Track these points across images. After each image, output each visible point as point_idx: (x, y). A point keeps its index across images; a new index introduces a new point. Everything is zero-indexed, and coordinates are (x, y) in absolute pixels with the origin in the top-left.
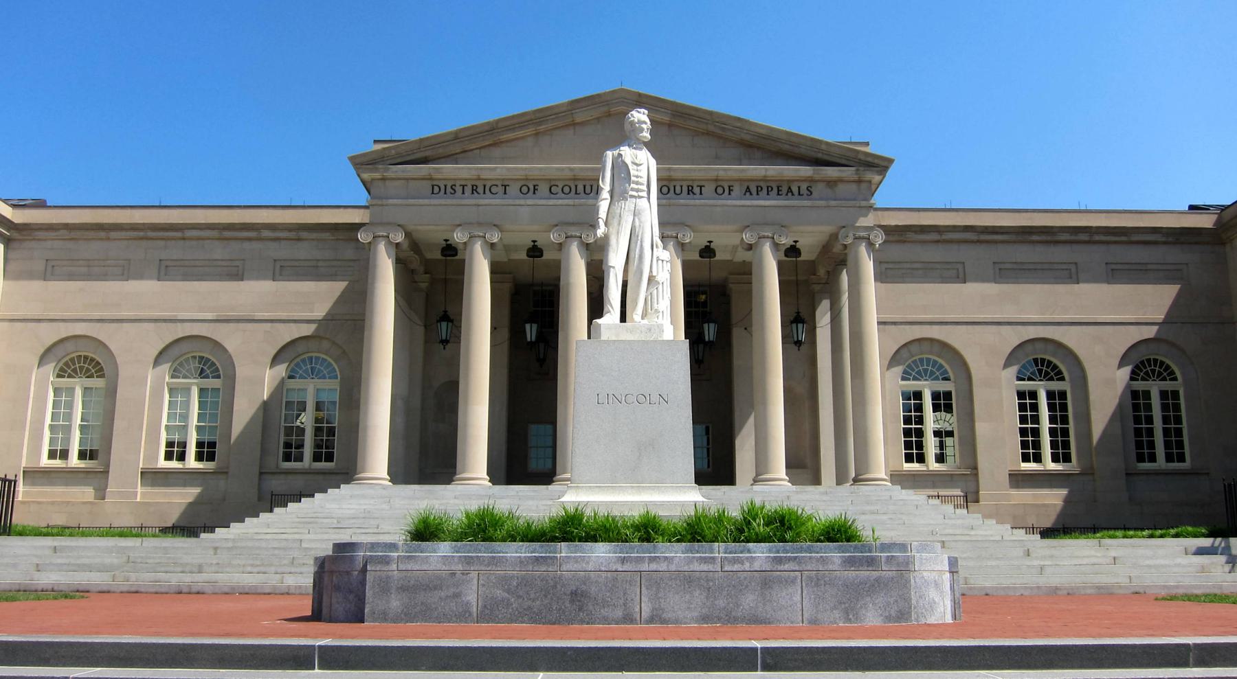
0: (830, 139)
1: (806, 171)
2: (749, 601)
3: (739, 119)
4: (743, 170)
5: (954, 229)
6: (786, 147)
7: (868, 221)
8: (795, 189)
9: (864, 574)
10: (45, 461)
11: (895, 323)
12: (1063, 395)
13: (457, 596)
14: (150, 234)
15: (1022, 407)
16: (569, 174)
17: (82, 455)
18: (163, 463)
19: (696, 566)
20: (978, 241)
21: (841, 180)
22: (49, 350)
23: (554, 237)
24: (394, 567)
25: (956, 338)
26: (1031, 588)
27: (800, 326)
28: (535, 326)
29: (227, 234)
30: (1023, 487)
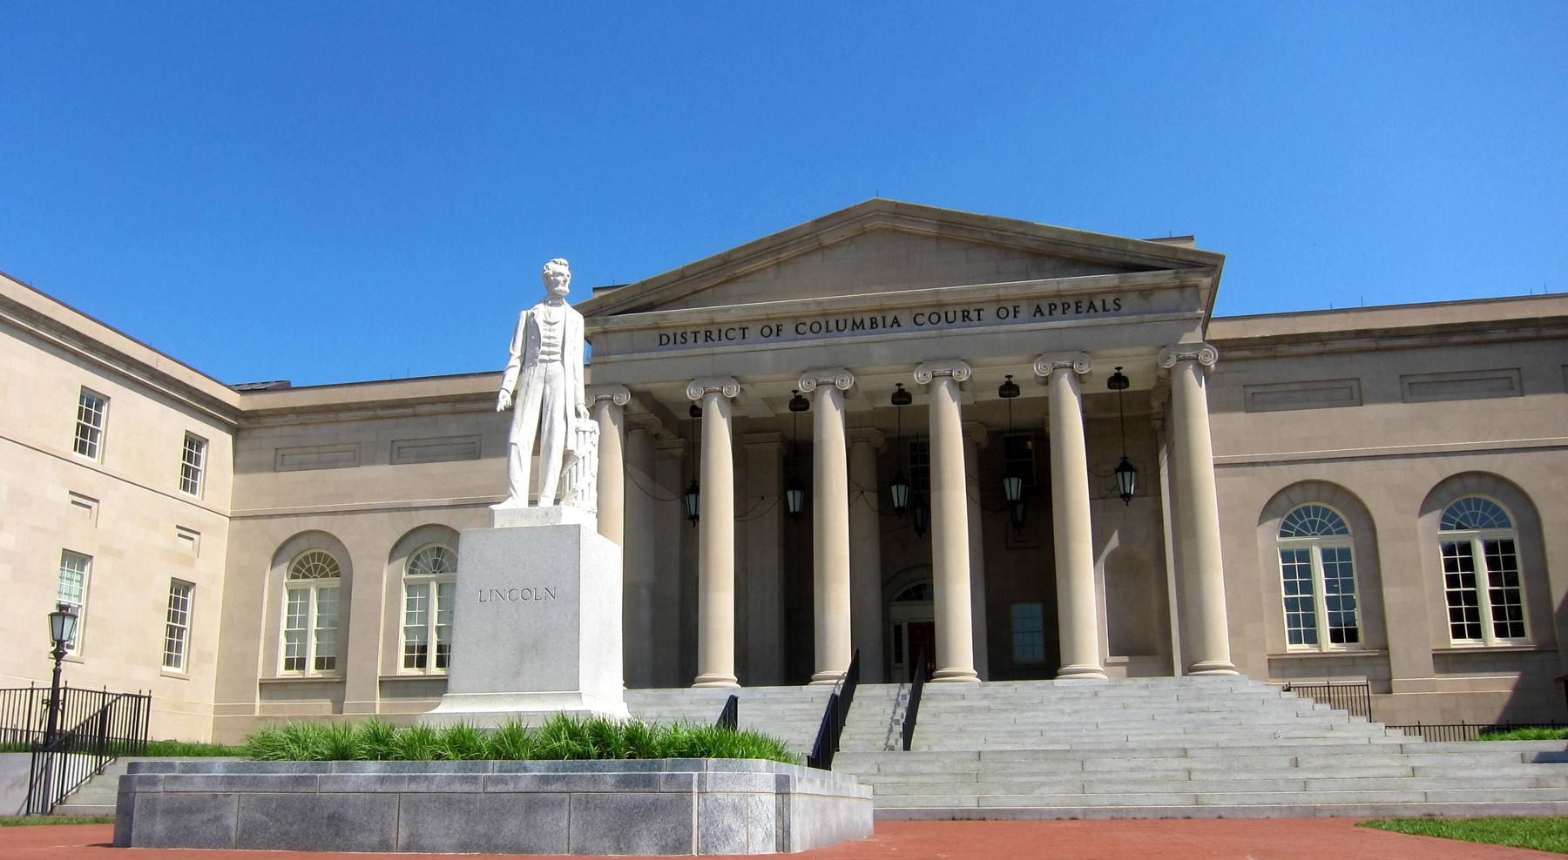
0: (1139, 237)
1: (1110, 280)
2: (512, 826)
3: (1020, 223)
4: (1029, 286)
5: (1342, 335)
6: (1083, 252)
7: (1195, 337)
8: (1098, 304)
9: (641, 796)
10: (282, 672)
11: (1266, 464)
12: (1508, 546)
13: (217, 819)
14: (380, 413)
15: (1450, 565)
16: (814, 309)
17: (320, 664)
18: (402, 671)
19: (457, 787)
20: (1377, 350)
21: (1157, 288)
22: (281, 549)
23: (919, 377)
24: (161, 788)
25: (1352, 478)
26: (1280, 809)
27: (1127, 474)
28: (798, 494)
29: (459, 406)
30: (1455, 672)
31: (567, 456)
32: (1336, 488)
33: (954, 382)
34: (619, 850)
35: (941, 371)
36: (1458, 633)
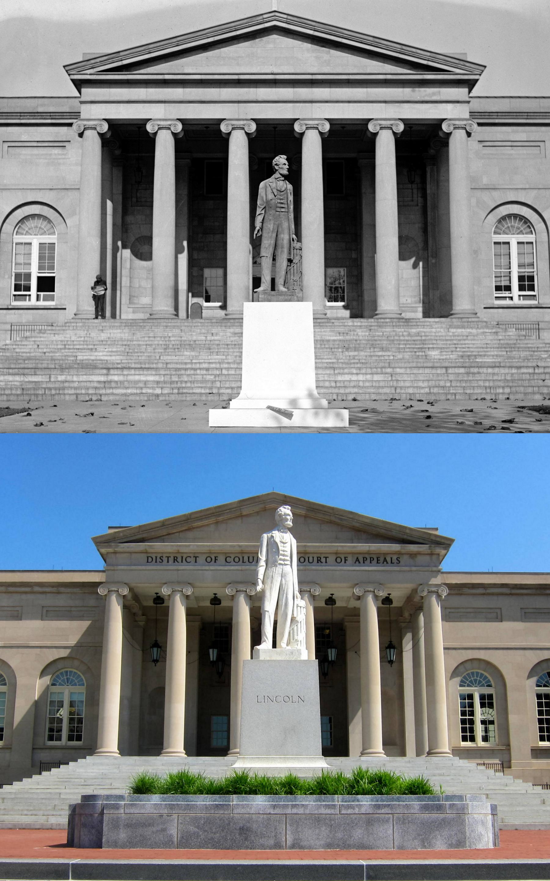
1: (396, 547)
3: (351, 513)
4: (354, 547)
5: (495, 586)
6: (382, 531)
8: (389, 559)
9: (435, 816)
13: (164, 830)
16: (238, 549)
20: (511, 594)
21: (419, 553)
23: (228, 591)
26: (546, 825)
27: (392, 650)
29: (11, 589)
30: (540, 758)
31: (293, 619)
32: (488, 664)
33: (183, 595)
34: (425, 847)
35: (305, 589)
36: (464, 739)
